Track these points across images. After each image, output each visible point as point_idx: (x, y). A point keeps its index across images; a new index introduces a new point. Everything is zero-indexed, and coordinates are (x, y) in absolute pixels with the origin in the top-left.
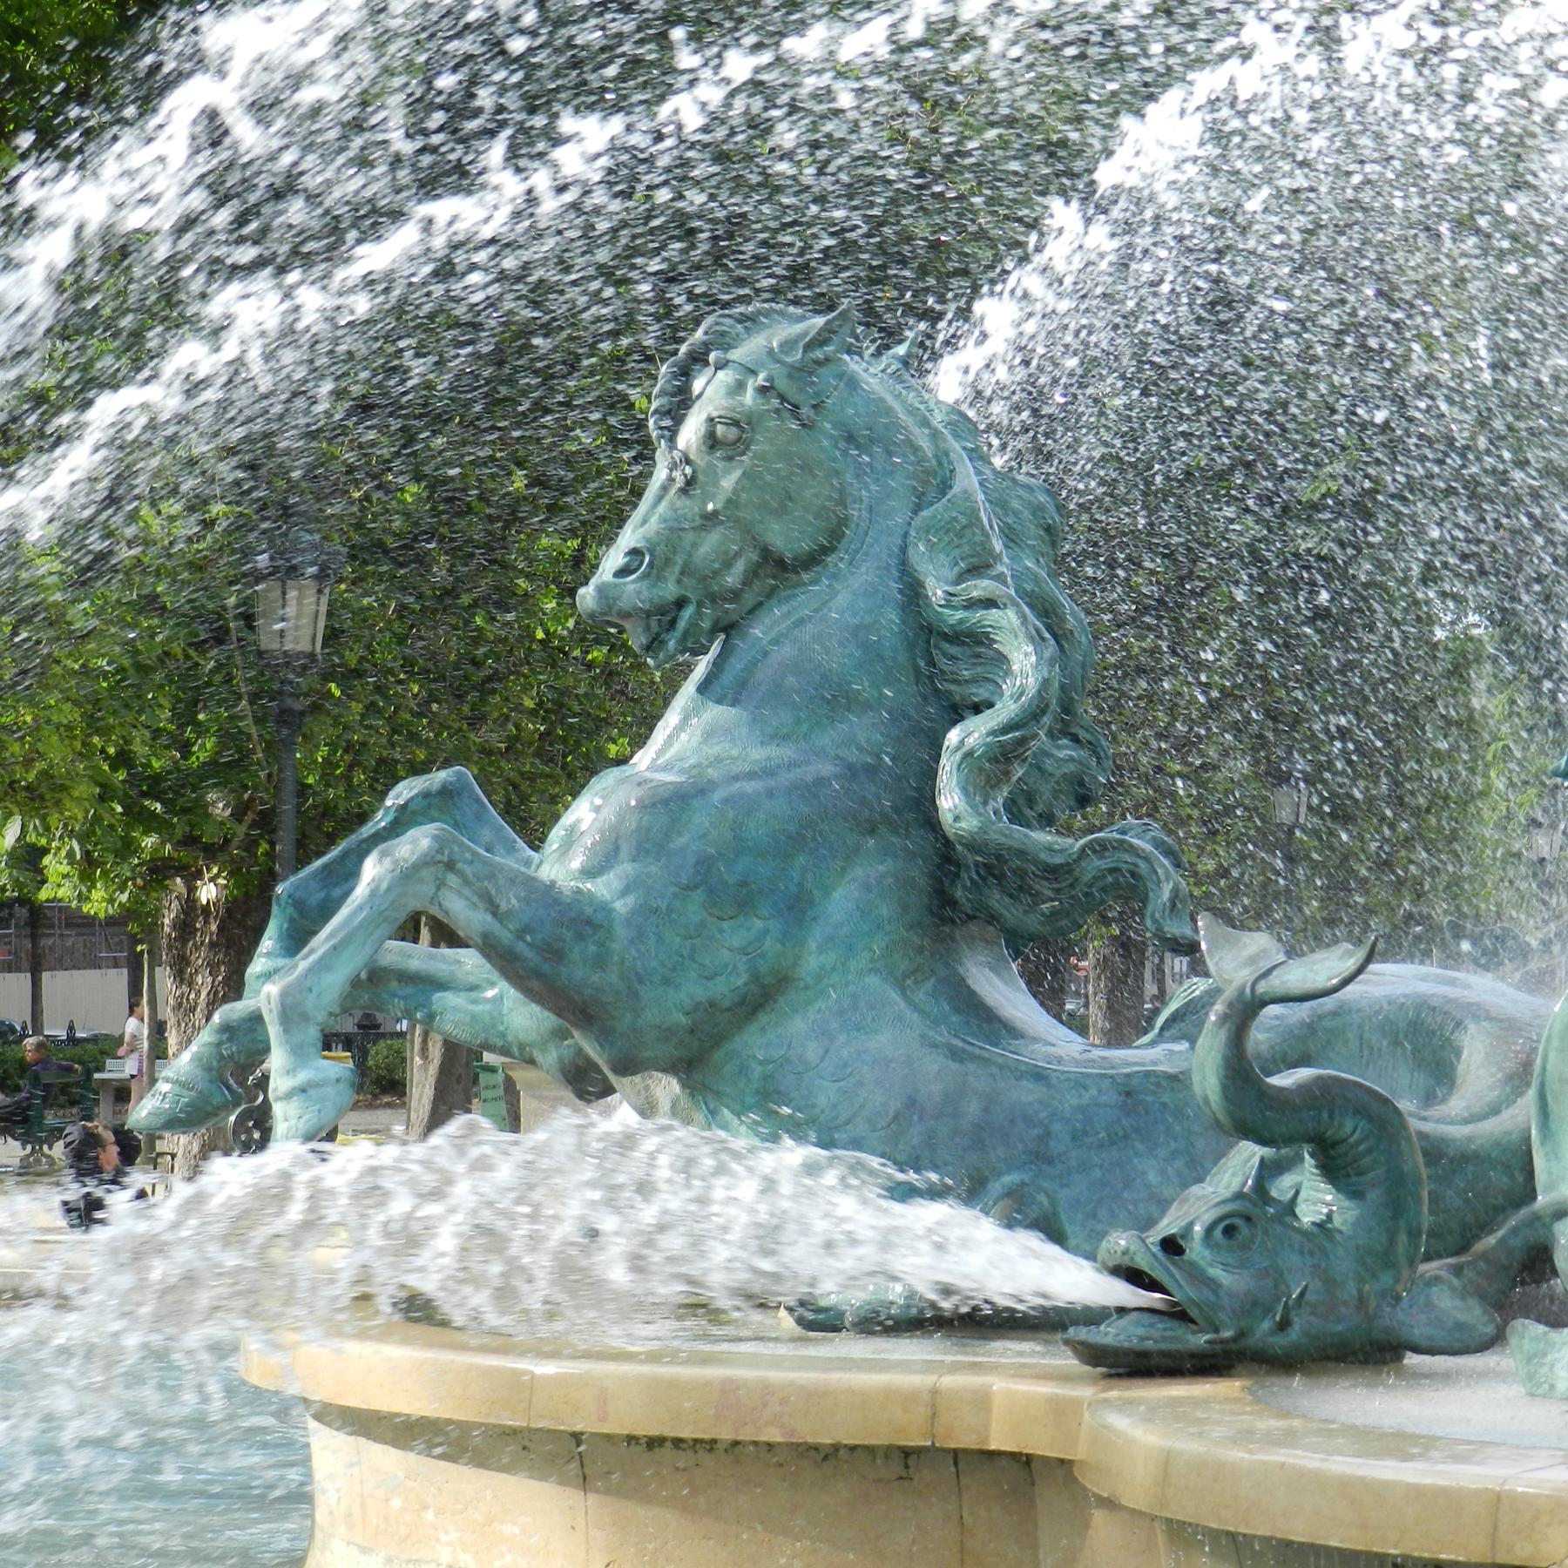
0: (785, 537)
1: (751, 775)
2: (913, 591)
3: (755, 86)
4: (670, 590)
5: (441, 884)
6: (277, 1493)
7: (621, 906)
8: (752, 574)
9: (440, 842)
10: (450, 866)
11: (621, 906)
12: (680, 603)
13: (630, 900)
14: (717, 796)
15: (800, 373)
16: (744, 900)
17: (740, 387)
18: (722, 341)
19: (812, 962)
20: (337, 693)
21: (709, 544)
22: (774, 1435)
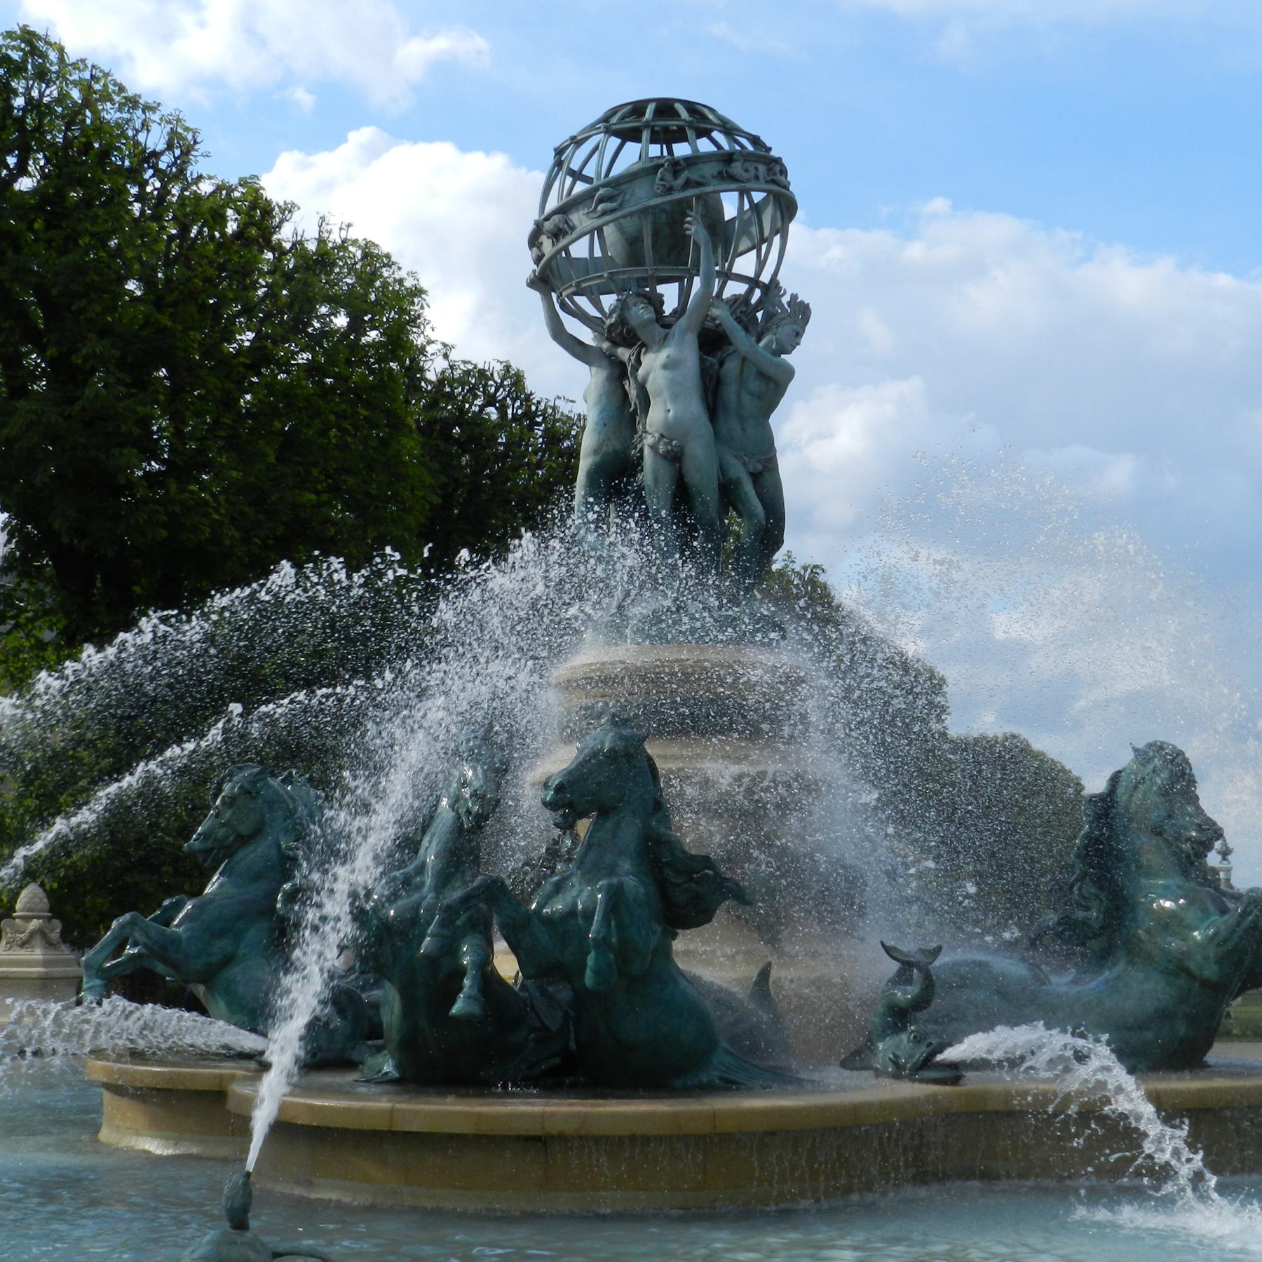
0: (244, 829)
1: (228, 898)
2: (279, 845)
3: (759, 849)
4: (209, 844)
5: (133, 930)
6: (1233, 1070)
7: (184, 936)
8: (235, 841)
9: (133, 918)
10: (136, 924)
11: (184, 936)
12: (213, 849)
13: (188, 933)
14: (215, 904)
15: (254, 783)
16: (221, 934)
17: (234, 787)
18: (231, 775)
19: (242, 951)
20: (459, 922)
21: (222, 831)
22: (181, 1087)
